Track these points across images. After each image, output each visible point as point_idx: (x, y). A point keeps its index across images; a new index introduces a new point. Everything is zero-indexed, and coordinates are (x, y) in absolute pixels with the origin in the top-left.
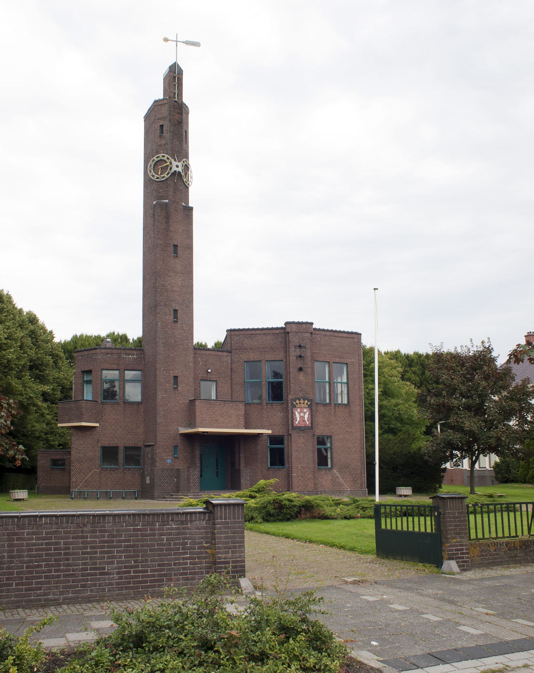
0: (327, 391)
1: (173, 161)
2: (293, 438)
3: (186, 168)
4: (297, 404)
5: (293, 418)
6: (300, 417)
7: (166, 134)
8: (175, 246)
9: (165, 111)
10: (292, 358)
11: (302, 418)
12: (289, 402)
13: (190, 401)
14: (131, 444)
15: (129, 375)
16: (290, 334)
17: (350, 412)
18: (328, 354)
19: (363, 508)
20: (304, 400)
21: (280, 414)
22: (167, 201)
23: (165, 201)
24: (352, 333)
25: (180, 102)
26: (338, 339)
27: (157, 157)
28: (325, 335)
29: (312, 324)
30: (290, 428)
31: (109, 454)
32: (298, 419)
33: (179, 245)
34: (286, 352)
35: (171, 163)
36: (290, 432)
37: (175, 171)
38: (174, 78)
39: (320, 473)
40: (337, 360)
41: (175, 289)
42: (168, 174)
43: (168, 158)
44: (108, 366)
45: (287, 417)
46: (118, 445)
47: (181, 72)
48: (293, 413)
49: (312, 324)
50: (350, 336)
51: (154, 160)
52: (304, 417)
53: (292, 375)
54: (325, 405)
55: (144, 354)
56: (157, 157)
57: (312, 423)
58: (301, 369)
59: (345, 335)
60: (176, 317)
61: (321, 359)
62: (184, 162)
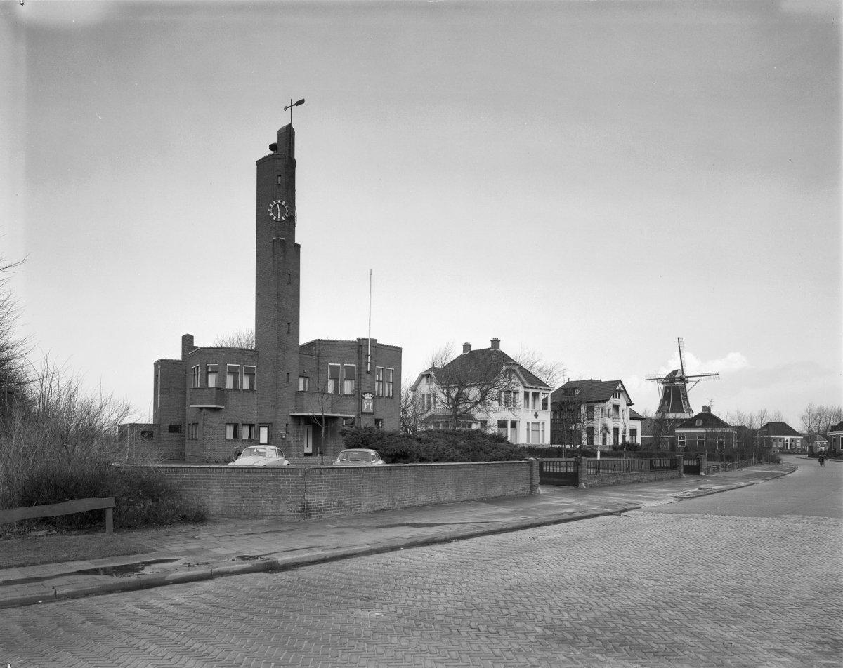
29: (376, 340)
49: (376, 340)
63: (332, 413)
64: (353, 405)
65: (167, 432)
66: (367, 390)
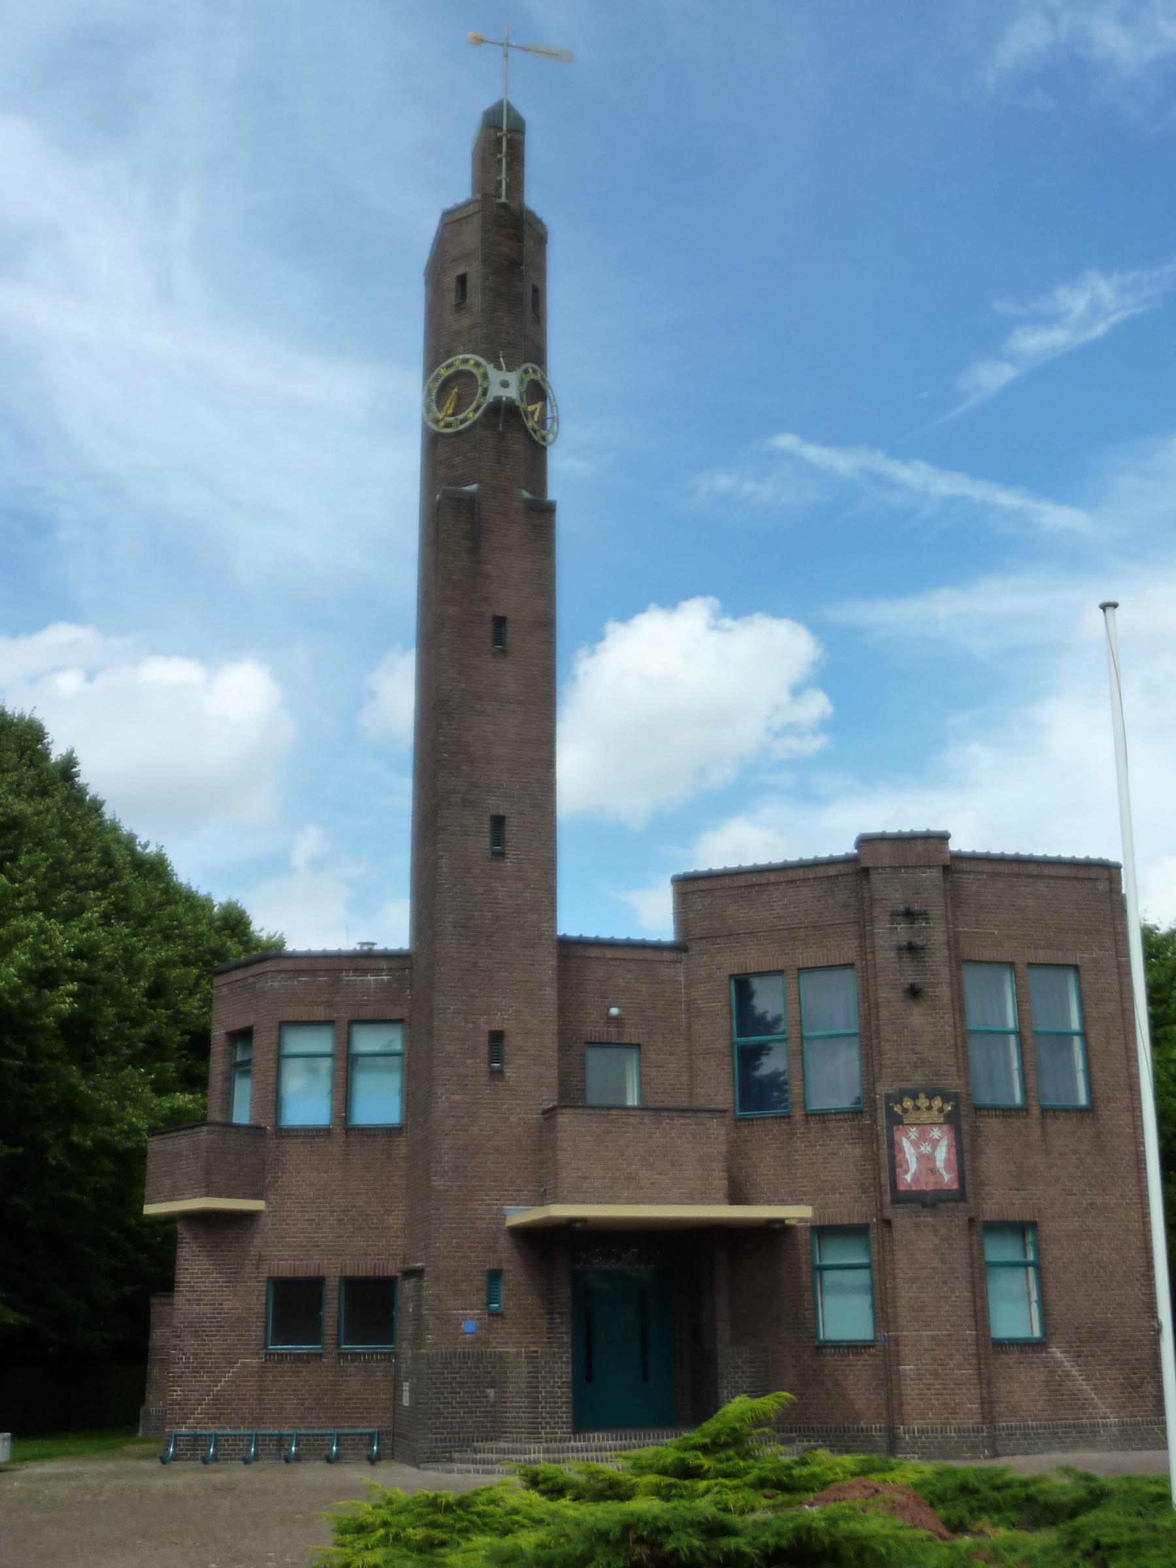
0: (1015, 1064)
1: (490, 369)
2: (897, 1235)
3: (537, 391)
4: (905, 1111)
5: (894, 1164)
6: (921, 1157)
7: (476, 299)
8: (500, 622)
9: (472, 237)
10: (885, 956)
11: (927, 1160)
12: (881, 1104)
13: (545, 1112)
14: (363, 1267)
15: (367, 1041)
16: (874, 877)
19: (1097, 1546)
20: (930, 1097)
21: (853, 1151)
22: (473, 487)
23: (468, 488)
24: (1088, 864)
25: (514, 205)
27: (448, 367)
29: (944, 838)
30: (887, 1198)
31: (294, 1306)
32: (913, 1165)
33: (511, 616)
34: (862, 936)
35: (485, 376)
36: (888, 1213)
37: (498, 400)
38: (502, 144)
40: (1042, 956)
42: (476, 411)
43: (478, 365)
44: (300, 1013)
45: (875, 1160)
46: (324, 1272)
47: (517, 128)
48: (892, 1144)
49: (944, 838)
50: (1082, 873)
51: (439, 375)
52: (931, 1158)
53: (884, 1014)
54: (1007, 1112)
55: (411, 968)
56: (448, 367)
57: (961, 1179)
58: (914, 992)
61: (985, 955)
62: (526, 371)
63: (736, 1196)
64: (843, 1157)
65: (487, 1028)
66: (918, 1079)
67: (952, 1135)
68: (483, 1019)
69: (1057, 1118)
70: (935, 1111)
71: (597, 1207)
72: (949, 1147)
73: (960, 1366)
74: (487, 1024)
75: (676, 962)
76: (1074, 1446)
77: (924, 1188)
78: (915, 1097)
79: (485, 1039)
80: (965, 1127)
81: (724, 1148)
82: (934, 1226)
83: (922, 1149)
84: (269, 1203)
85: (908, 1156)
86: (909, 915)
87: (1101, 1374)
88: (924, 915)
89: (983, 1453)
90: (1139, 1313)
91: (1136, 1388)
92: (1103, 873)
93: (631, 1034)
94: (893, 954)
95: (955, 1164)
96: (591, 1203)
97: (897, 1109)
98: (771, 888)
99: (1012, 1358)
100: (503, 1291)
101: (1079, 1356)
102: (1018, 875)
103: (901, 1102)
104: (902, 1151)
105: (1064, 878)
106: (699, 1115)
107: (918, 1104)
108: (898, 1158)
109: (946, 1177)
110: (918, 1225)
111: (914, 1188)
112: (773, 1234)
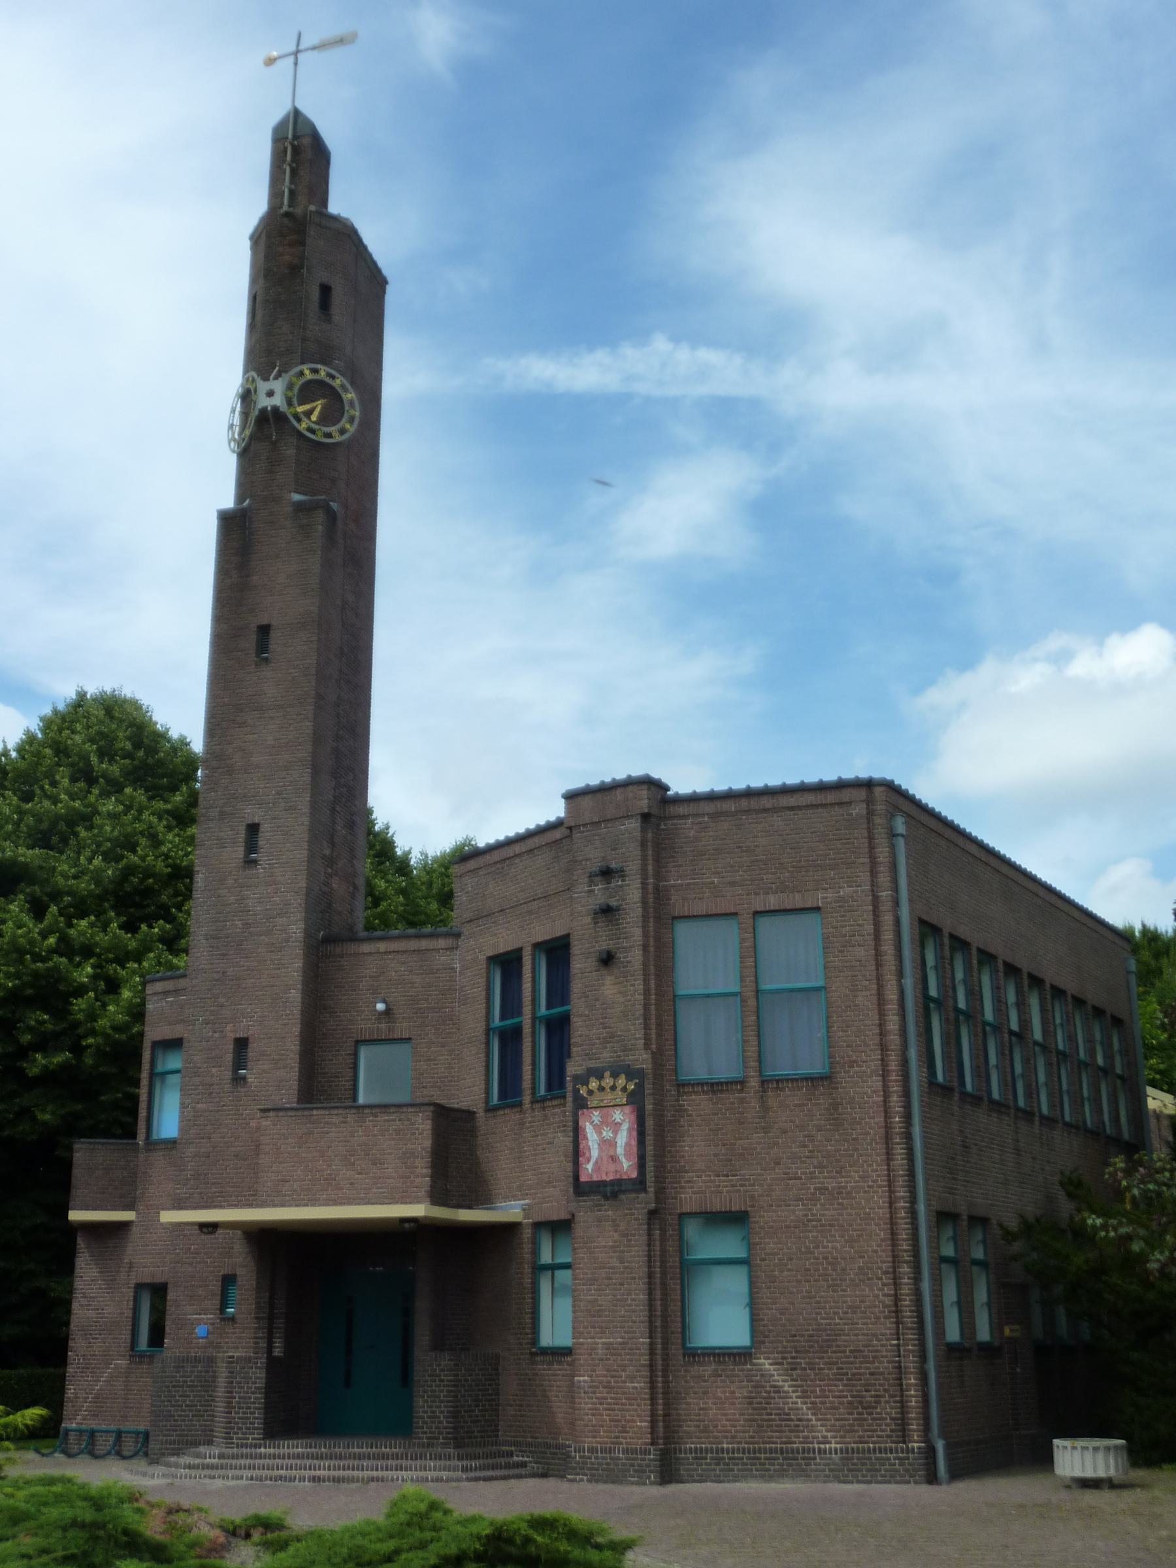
4: (590, 1092)
17: (835, 1105)
18: (732, 884)
20: (615, 1075)
26: (777, 821)
28: (715, 816)
33: (274, 623)
37: (264, 411)
38: (300, 156)
39: (696, 1370)
40: (773, 902)
41: (255, 759)
50: (831, 797)
52: (612, 1144)
58: (607, 960)
59: (809, 798)
60: (251, 846)
61: (700, 908)
66: (606, 1056)
67: (633, 1117)
68: (229, 1027)
69: (782, 1090)
70: (619, 1092)
71: (323, 1208)
72: (630, 1130)
73: (632, 1378)
74: (232, 1032)
75: (451, 949)
76: (781, 1474)
77: (604, 1178)
78: (600, 1077)
79: (231, 1047)
80: (649, 1107)
81: (428, 1143)
82: (614, 1221)
83: (604, 1134)
84: (138, 1214)
85: (590, 1144)
86: (607, 873)
87: (822, 1391)
88: (621, 873)
89: (649, 1478)
90: (878, 1318)
91: (869, 1407)
92: (862, 794)
93: (402, 1028)
94: (588, 919)
95: (635, 1149)
96: (290, 1206)
97: (583, 1091)
98: (517, 861)
99: (708, 1369)
100: (235, 1293)
101: (794, 1369)
102: (747, 812)
103: (587, 1084)
104: (585, 1138)
105: (807, 807)
106: (405, 1109)
107: (603, 1084)
108: (581, 1146)
109: (626, 1165)
110: (599, 1220)
111: (595, 1179)
112: (509, 1229)
